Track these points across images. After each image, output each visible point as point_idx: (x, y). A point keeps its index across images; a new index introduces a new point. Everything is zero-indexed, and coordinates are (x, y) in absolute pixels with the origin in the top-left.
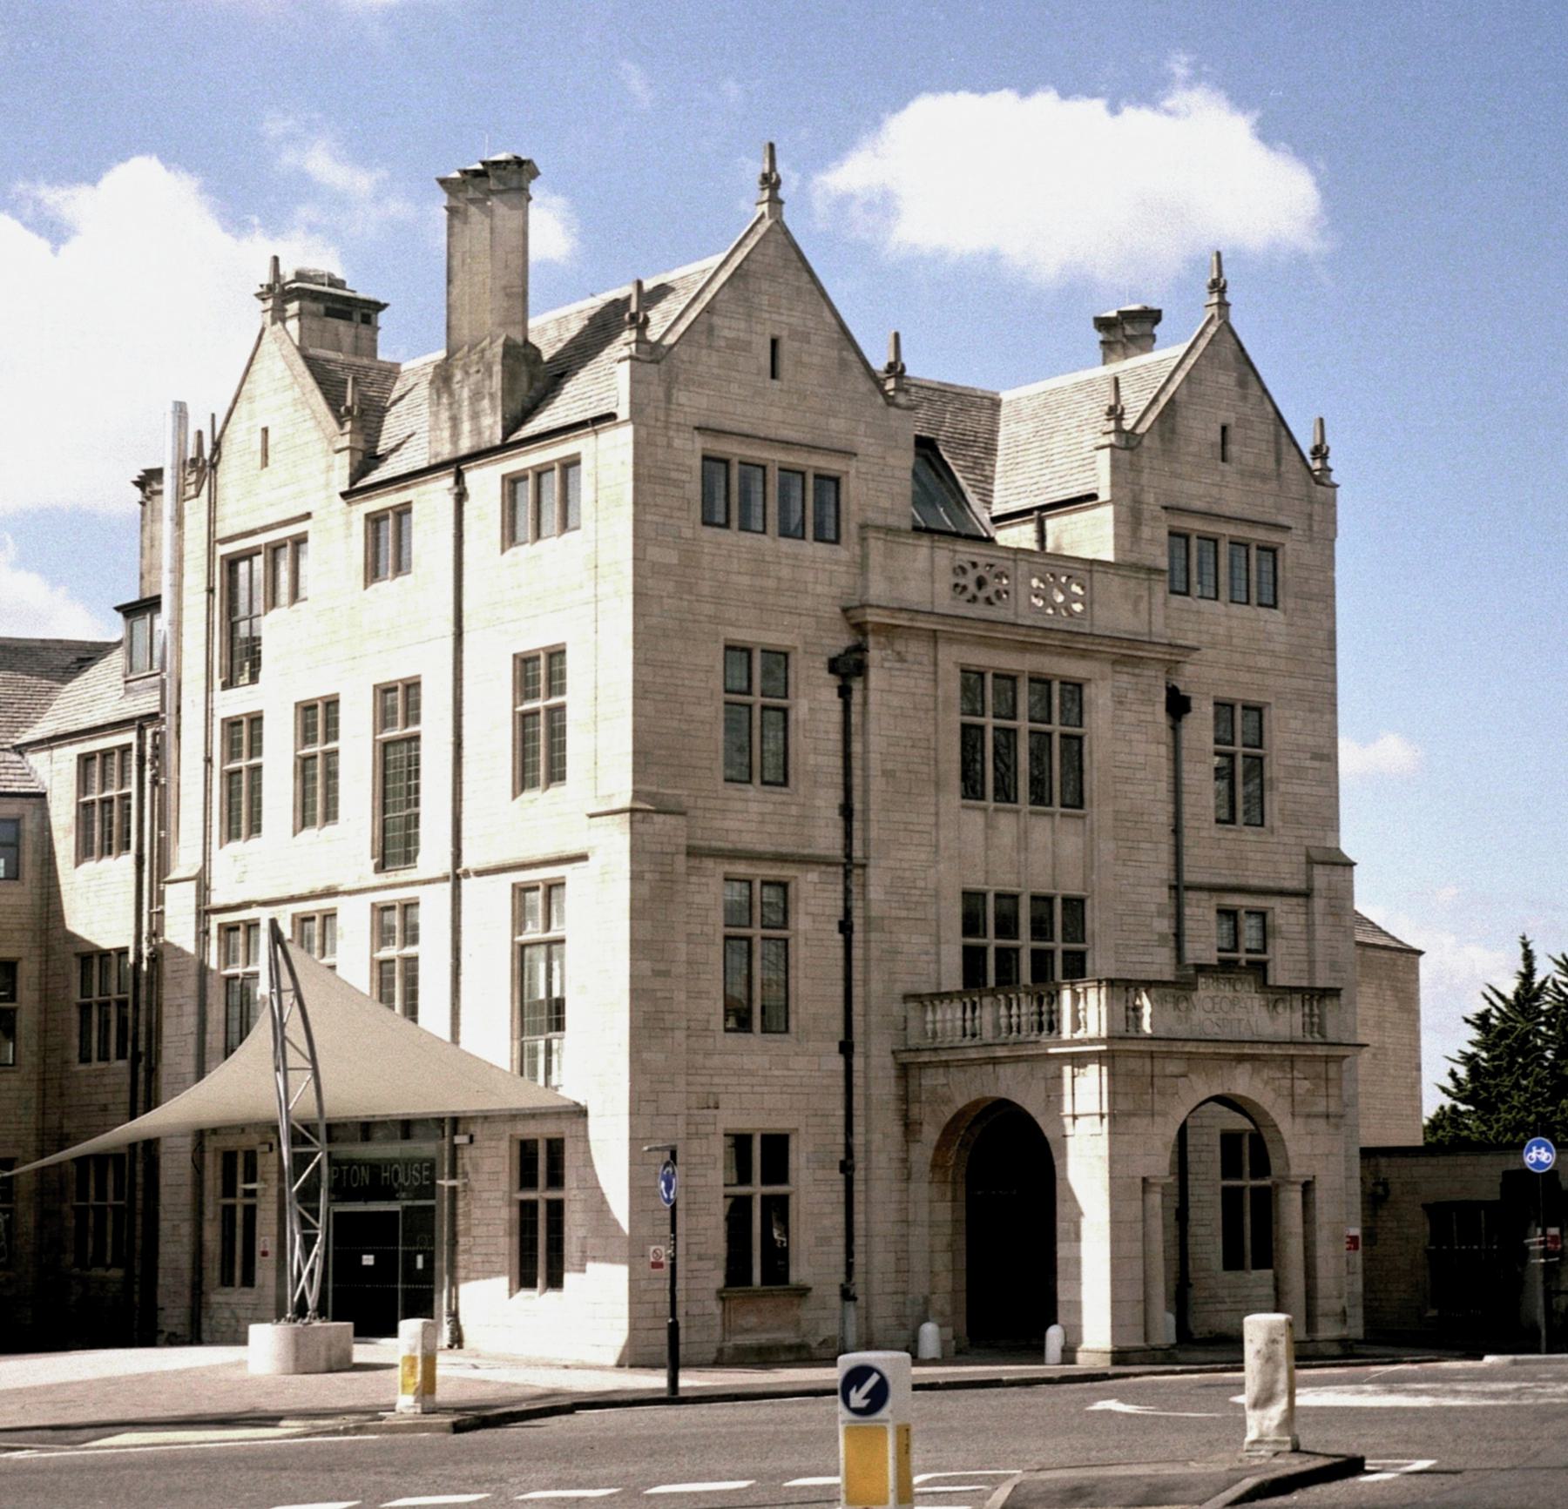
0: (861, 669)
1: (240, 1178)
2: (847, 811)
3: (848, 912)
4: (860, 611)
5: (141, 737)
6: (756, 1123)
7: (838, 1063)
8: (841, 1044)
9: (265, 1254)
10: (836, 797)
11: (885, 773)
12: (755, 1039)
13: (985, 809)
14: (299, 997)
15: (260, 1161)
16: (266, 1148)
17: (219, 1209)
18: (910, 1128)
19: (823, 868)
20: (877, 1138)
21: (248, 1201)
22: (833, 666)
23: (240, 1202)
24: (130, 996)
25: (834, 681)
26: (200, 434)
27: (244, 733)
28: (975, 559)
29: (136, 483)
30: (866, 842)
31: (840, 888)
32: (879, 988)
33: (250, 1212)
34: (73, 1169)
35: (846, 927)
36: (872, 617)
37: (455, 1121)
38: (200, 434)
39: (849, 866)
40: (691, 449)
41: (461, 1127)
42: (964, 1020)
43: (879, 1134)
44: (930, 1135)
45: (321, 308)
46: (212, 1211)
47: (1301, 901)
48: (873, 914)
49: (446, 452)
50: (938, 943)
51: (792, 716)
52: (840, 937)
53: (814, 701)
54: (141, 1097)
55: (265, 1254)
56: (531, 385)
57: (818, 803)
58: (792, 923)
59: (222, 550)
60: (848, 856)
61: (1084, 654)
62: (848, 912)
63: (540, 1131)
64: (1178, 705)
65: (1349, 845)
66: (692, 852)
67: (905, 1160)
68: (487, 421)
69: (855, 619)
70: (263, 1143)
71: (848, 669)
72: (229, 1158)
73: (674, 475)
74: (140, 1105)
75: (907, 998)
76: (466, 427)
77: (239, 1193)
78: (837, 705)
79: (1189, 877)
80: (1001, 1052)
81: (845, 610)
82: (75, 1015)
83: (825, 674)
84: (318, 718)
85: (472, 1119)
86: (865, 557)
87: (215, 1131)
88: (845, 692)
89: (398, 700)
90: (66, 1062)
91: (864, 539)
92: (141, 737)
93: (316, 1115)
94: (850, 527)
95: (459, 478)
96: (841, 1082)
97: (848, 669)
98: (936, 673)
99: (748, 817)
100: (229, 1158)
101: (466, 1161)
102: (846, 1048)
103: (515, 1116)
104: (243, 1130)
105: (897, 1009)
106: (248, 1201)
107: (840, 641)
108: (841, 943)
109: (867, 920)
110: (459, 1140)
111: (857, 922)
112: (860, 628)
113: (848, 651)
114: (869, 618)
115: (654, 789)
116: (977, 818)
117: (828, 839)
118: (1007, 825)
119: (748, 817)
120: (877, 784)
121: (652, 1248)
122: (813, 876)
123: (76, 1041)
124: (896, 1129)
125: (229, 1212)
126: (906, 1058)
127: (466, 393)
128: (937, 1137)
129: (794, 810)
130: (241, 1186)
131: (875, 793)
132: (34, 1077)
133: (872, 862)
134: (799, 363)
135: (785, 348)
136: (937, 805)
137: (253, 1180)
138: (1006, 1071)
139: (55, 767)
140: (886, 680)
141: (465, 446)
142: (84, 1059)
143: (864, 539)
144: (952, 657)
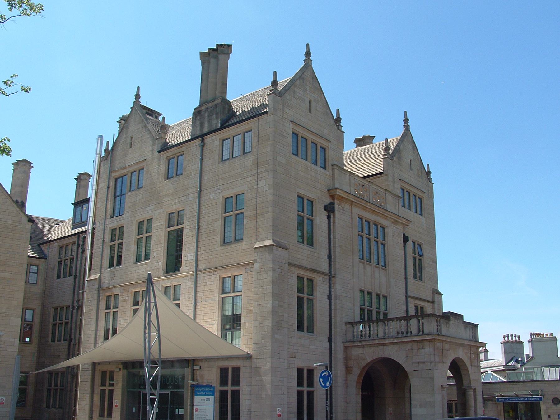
0: (333, 211)
1: (108, 380)
2: (330, 257)
3: (330, 292)
4: (334, 191)
5: (79, 238)
6: (305, 365)
7: (328, 344)
8: (328, 338)
9: (116, 406)
10: (326, 252)
11: (340, 246)
12: (305, 334)
13: (363, 263)
14: (156, 305)
15: (116, 374)
16: (118, 370)
17: (100, 390)
18: (348, 369)
19: (323, 276)
20: (339, 372)
21: (111, 388)
22: (326, 208)
23: (107, 388)
24: (70, 321)
25: (326, 213)
26: (108, 142)
27: (117, 234)
28: (360, 182)
29: (75, 179)
30: (335, 269)
31: (328, 284)
32: (340, 319)
33: (111, 392)
34: (47, 375)
35: (329, 297)
36: (339, 192)
37: (194, 360)
38: (108, 142)
39: (331, 277)
40: (289, 128)
41: (195, 363)
42: (370, 330)
43: (339, 370)
44: (356, 371)
45: (145, 111)
46: (97, 391)
47: (431, 304)
48: (337, 294)
49: (198, 133)
50: (354, 306)
51: (314, 223)
52: (328, 301)
53: (320, 219)
54: (71, 353)
55: (116, 406)
56: (228, 113)
57: (322, 253)
58: (315, 294)
59: (114, 175)
60: (330, 272)
61: (386, 218)
62: (330, 292)
63: (230, 364)
64: (406, 239)
65: (440, 290)
66: (290, 264)
67: (346, 380)
68: (214, 122)
69: (332, 193)
70: (117, 368)
71: (330, 209)
72: (104, 373)
73: (285, 134)
74: (71, 356)
75: (347, 323)
76: (206, 125)
77: (107, 384)
78: (326, 221)
79: (410, 294)
80: (388, 341)
81: (328, 190)
82: (51, 327)
83: (323, 210)
84: (144, 226)
85: (200, 360)
86: (333, 174)
87: (99, 363)
88: (329, 217)
89: (174, 219)
90: (47, 341)
91: (333, 169)
92: (79, 238)
93: (144, 358)
94: (329, 165)
95: (203, 141)
96: (328, 352)
97: (330, 209)
98: (352, 216)
99: (303, 255)
100: (104, 373)
101: (198, 375)
102: (330, 340)
103: (218, 359)
104: (110, 363)
105: (344, 328)
106: (111, 388)
107: (328, 201)
108: (328, 303)
109: (336, 296)
110: (195, 367)
111: (333, 296)
112: (333, 197)
113: (329, 204)
114: (338, 193)
115: (278, 240)
116: (361, 265)
117: (325, 267)
118: (369, 268)
119: (303, 255)
120: (338, 249)
121: (278, 409)
122: (321, 279)
123: (50, 335)
124: (344, 369)
125: (103, 391)
126: (347, 344)
127: (207, 114)
128: (359, 372)
129: (316, 255)
130: (108, 382)
131: (338, 253)
132: (37, 346)
133: (337, 276)
134: (316, 110)
135: (313, 104)
136: (353, 259)
137: (113, 380)
138: (390, 348)
139: (50, 250)
140: (342, 216)
141: (206, 130)
142: (53, 341)
143: (333, 169)
144: (357, 211)
